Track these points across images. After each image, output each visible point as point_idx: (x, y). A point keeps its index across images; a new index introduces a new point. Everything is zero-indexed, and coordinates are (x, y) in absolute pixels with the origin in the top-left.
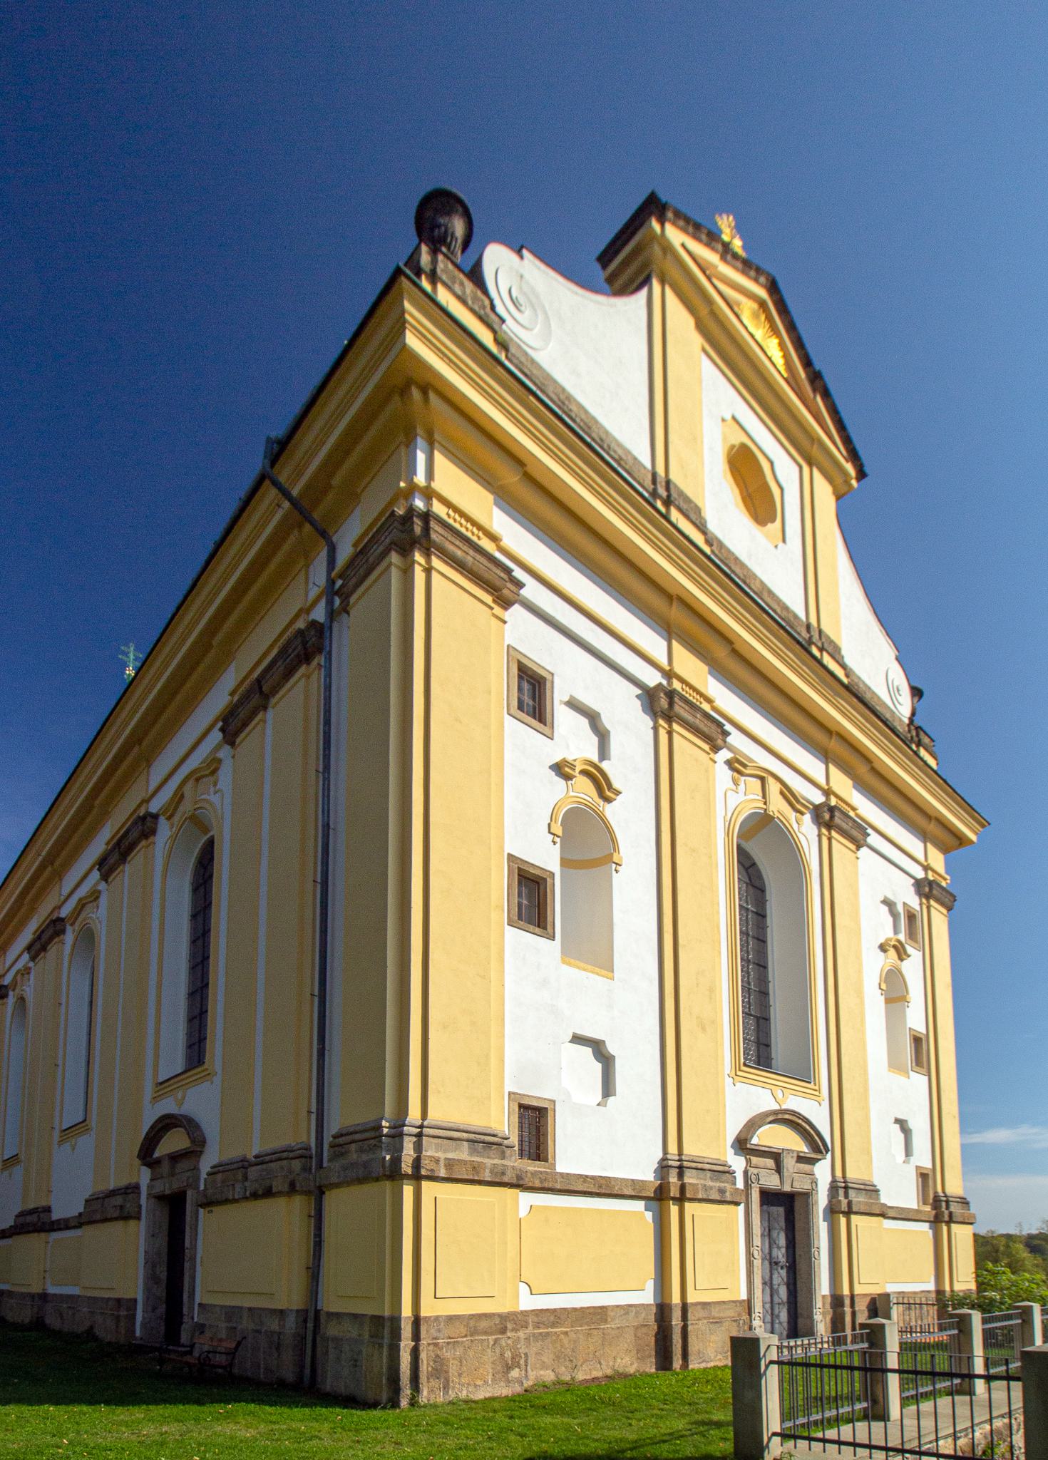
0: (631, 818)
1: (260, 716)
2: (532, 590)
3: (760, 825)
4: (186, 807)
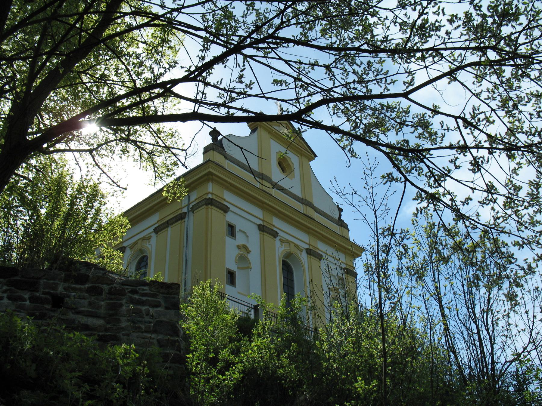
0: (254, 257)
1: (166, 229)
2: (232, 208)
3: (289, 255)
4: (138, 246)
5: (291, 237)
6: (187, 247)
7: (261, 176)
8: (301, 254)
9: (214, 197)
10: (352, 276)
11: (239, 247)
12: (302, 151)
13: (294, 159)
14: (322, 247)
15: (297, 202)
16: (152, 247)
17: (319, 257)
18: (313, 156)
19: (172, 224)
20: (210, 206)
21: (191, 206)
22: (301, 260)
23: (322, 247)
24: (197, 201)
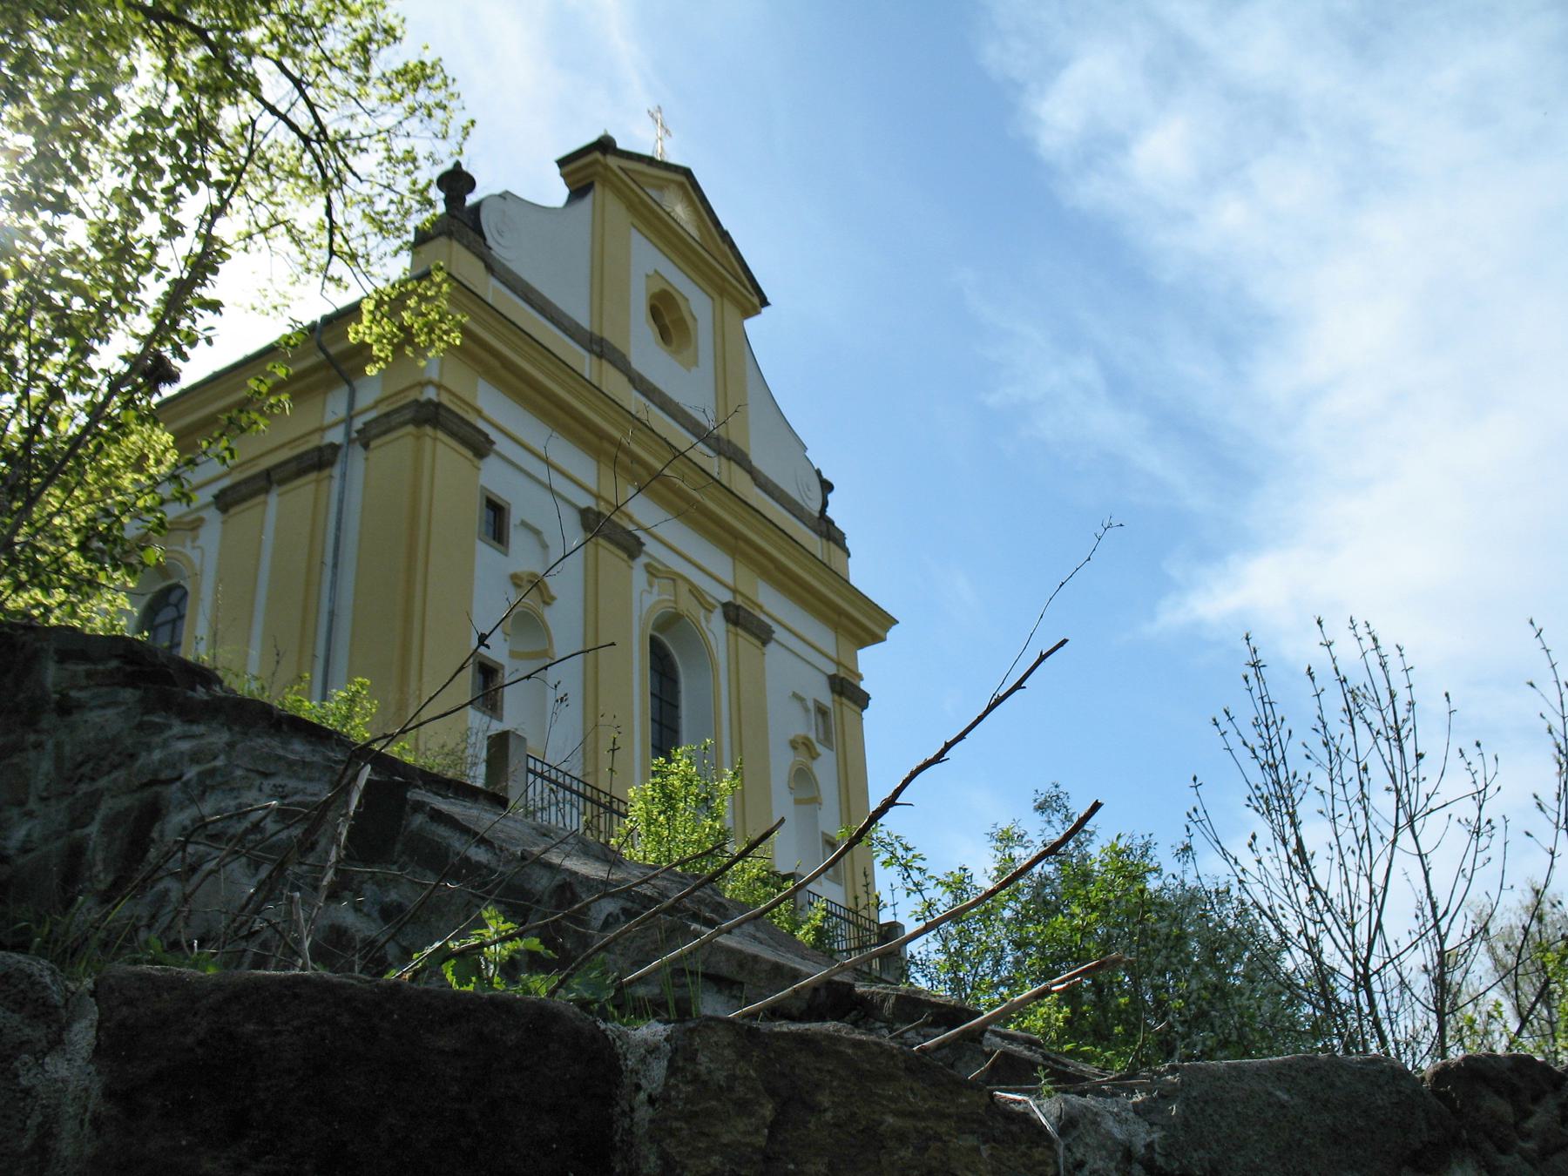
0: (564, 622)
1: (261, 498)
2: (780, 634)
3: (670, 621)
5: (681, 561)
6: (335, 565)
7: (599, 347)
8: (708, 621)
9: (445, 399)
10: (855, 702)
11: (516, 580)
12: (724, 279)
13: (698, 303)
14: (771, 602)
15: (567, 339)
16: (204, 556)
17: (763, 635)
18: (756, 300)
19: (281, 482)
20: (428, 429)
21: (358, 424)
22: (708, 645)
23: (771, 602)
24: (383, 409)
